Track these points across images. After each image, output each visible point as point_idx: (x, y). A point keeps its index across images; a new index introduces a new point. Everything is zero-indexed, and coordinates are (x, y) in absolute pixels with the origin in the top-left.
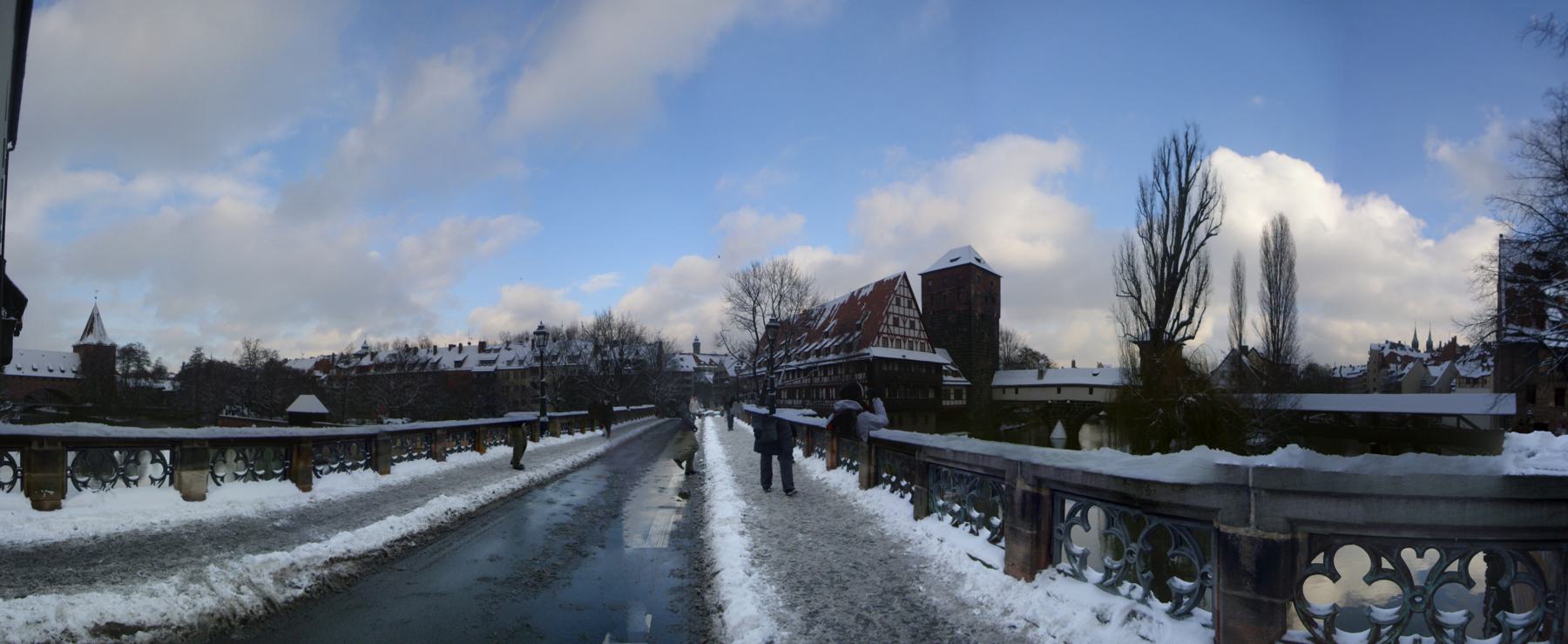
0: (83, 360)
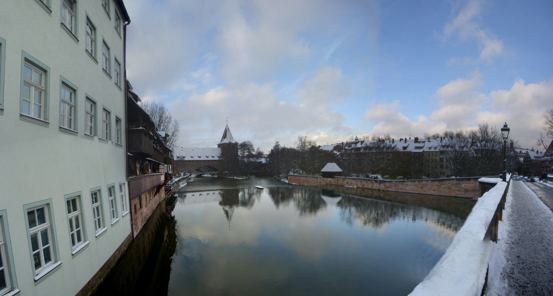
0: (222, 151)
